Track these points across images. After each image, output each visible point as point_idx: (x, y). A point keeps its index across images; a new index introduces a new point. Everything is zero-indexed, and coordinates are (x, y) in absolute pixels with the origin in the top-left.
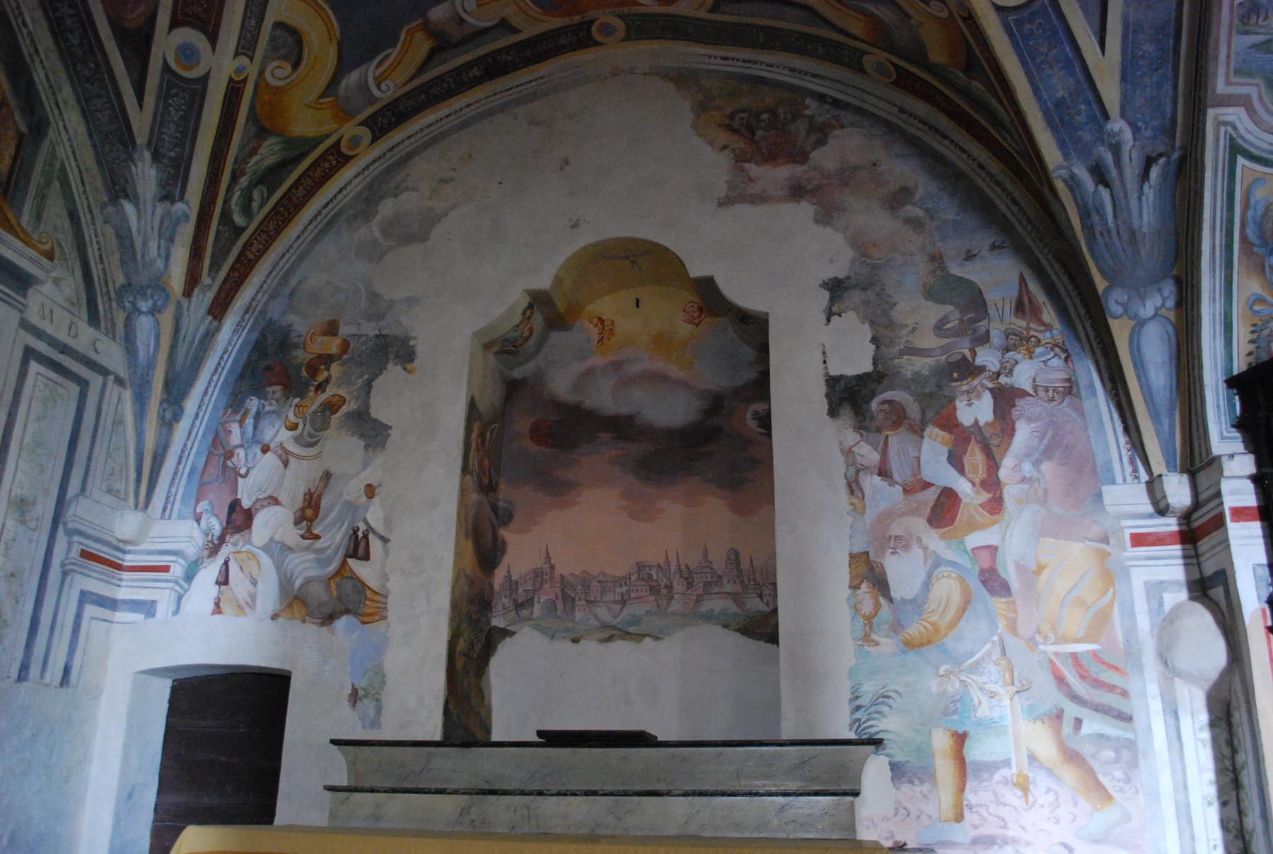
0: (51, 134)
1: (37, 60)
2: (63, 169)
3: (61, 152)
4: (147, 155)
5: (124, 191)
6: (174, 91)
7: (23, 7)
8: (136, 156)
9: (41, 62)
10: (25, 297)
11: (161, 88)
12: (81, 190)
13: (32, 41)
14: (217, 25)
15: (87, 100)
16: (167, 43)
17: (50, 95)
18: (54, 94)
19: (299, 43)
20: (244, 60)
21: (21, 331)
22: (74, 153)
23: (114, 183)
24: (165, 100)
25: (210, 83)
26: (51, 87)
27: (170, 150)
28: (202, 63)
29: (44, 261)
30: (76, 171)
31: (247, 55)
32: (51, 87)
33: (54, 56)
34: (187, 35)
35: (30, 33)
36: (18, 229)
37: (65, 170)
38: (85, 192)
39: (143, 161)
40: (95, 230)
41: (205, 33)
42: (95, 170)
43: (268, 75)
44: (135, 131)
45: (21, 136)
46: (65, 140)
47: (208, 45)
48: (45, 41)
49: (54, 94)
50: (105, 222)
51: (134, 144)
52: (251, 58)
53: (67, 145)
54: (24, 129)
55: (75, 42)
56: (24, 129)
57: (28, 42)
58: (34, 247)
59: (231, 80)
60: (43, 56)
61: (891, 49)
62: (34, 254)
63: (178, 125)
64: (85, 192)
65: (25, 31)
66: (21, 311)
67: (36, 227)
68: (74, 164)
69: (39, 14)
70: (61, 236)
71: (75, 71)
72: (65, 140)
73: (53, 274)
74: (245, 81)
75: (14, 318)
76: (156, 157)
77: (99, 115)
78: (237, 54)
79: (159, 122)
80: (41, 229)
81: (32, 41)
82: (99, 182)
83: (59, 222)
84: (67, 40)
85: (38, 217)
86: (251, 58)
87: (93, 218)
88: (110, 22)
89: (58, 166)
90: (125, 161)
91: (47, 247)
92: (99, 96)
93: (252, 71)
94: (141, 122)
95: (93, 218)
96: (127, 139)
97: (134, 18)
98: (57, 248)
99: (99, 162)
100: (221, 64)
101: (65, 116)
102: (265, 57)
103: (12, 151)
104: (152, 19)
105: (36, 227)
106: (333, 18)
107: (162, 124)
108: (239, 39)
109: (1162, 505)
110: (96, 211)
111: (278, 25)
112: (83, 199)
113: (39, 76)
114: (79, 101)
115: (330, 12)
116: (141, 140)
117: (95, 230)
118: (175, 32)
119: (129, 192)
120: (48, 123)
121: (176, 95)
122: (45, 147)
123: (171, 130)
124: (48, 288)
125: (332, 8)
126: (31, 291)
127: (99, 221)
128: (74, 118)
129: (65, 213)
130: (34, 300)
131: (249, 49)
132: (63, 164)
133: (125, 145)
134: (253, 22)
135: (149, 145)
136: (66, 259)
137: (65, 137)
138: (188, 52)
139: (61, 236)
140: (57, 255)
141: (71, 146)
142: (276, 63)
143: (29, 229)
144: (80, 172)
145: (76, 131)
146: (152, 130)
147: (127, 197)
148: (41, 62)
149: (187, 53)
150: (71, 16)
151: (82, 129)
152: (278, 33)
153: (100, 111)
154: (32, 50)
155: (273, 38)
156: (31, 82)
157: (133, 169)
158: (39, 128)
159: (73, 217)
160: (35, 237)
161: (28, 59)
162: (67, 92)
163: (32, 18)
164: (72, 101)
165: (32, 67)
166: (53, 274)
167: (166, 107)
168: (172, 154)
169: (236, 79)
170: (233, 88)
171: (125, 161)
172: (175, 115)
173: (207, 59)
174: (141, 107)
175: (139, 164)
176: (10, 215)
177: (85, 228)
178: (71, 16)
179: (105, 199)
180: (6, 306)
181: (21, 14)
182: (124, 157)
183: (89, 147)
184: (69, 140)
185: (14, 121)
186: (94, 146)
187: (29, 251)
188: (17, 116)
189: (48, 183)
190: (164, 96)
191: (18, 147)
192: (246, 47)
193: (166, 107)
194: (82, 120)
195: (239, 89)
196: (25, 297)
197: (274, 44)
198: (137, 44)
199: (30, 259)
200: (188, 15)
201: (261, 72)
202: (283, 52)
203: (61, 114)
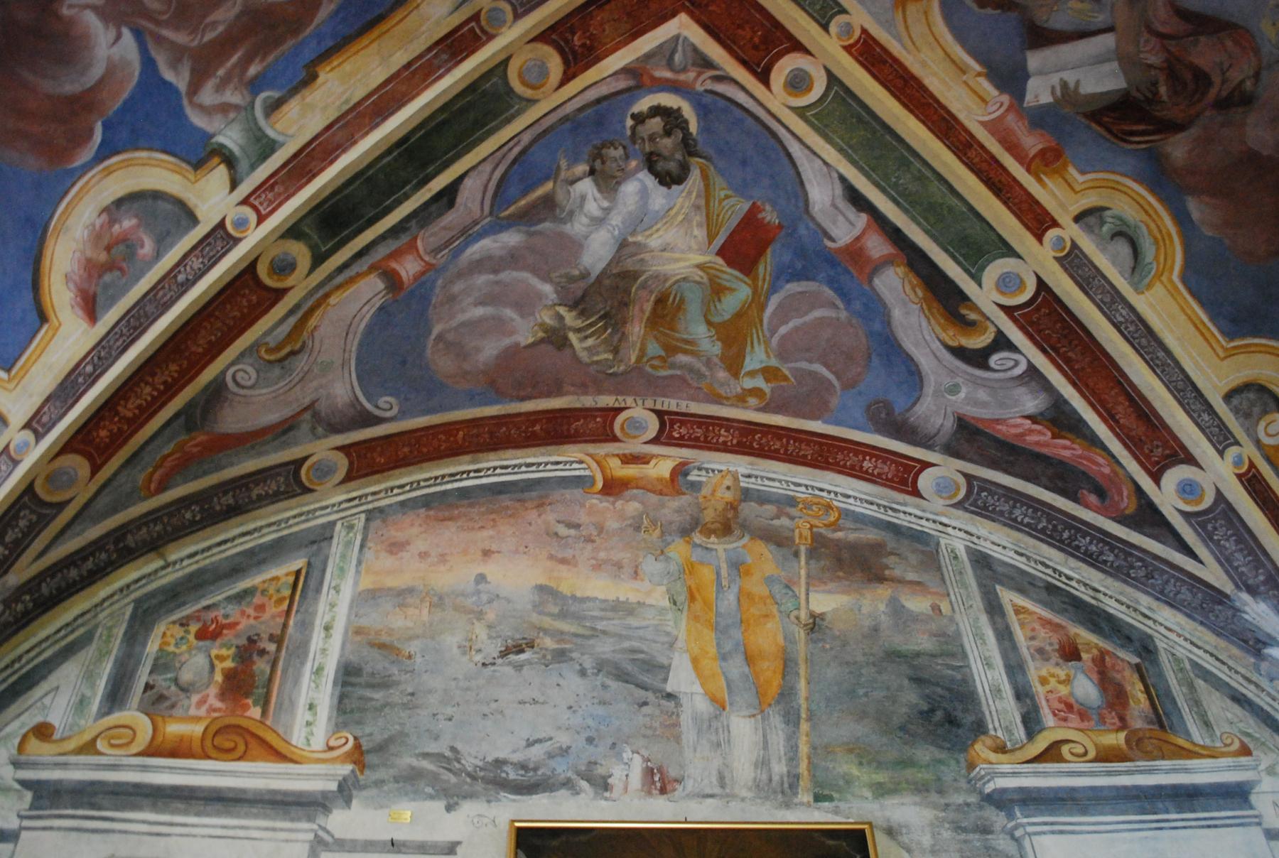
0: (1161, 645)
1: (1101, 596)
2: (1195, 665)
3: (1180, 652)
4: (1245, 596)
5: (1258, 641)
6: (1210, 527)
7: (1059, 568)
8: (1238, 604)
9: (1105, 594)
10: (1251, 808)
11: (1199, 534)
12: (1225, 668)
13: (1085, 585)
14: (1183, 447)
15: (1162, 592)
16: (1167, 495)
17: (1133, 614)
18: (1135, 610)
19: (1262, 389)
20: (1232, 452)
21: (1273, 843)
22: (1192, 643)
23: (1246, 642)
24: (1211, 539)
25: (1226, 494)
26: (1128, 607)
27: (1256, 576)
28: (1205, 486)
29: (1244, 760)
30: (1207, 657)
31: (1232, 445)
32: (1128, 607)
33: (1110, 581)
34: (1173, 477)
35: (1079, 582)
36: (1197, 749)
37: (1197, 664)
38: (1230, 668)
39: (1246, 604)
40: (1269, 694)
41: (1182, 462)
42: (1222, 643)
43: (1266, 441)
44: (1216, 585)
45: (1138, 668)
46: (1177, 639)
47: (1194, 469)
48: (1095, 577)
49: (1135, 610)
50: (1272, 680)
51: (1227, 596)
52: (1237, 443)
53: (1180, 641)
54: (1135, 660)
55: (1111, 558)
56: (1135, 660)
57: (1083, 589)
58: (1224, 755)
59: (1239, 476)
60: (1102, 589)
61: (335, 429)
62: (1229, 761)
63: (1241, 550)
64: (1230, 668)
65: (1074, 583)
66: (1259, 824)
67: (1212, 735)
68: (1200, 652)
69: (1073, 562)
70: (1241, 725)
71: (1133, 579)
72: (1177, 639)
73: (1262, 767)
74: (1252, 465)
75: (1256, 834)
76: (1252, 591)
77: (1179, 596)
78: (1221, 453)
79: (1225, 561)
80: (1218, 734)
81: (1085, 585)
82: (1235, 651)
83: (1229, 716)
84: (1105, 562)
85: (1207, 724)
86: (1237, 443)
87: (1257, 686)
88: (1119, 522)
89: (1188, 666)
90: (1234, 616)
91: (1236, 745)
92: (1167, 582)
93: (1249, 450)
94: (1212, 573)
95: (1257, 686)
96: (1219, 597)
97: (1128, 504)
98: (1246, 740)
99: (1218, 635)
100: (1218, 472)
101: (1161, 620)
102: (1247, 431)
103: (1140, 686)
104: (1139, 490)
105: (1212, 735)
106: (1263, 341)
107: (1228, 560)
108: (1210, 441)
109: (371, 759)
110: (1255, 677)
111: (1228, 397)
112: (1234, 676)
113: (1112, 607)
114: (1158, 599)
115: (1256, 341)
116: (1228, 588)
117: (1269, 694)
118: (1164, 481)
119: (1263, 639)
120: (1150, 637)
121: (1215, 529)
122: (1164, 658)
123: (1239, 559)
124: (1267, 784)
125: (1255, 336)
126: (1253, 798)
127: (1265, 683)
128: (1166, 615)
129: (1228, 701)
130: (1262, 802)
131: (1226, 439)
132: (1190, 660)
133: (1221, 603)
134: (1206, 417)
135: (1237, 586)
136: (1263, 744)
137: (1172, 636)
138: (1188, 488)
139: (1241, 725)
140: (1251, 746)
141: (1186, 639)
142: (1262, 424)
143: (1208, 742)
144: (1212, 655)
145: (1178, 624)
146: (1227, 572)
147: (1265, 644)
148: (1105, 594)
149: (1187, 489)
150: (1091, 543)
151: (1181, 618)
152: (1235, 401)
153: (1178, 592)
154: (1091, 593)
155: (1236, 411)
156: (1110, 618)
157: (1246, 617)
158: (1146, 648)
159: (1239, 699)
160: (1218, 744)
161: (1093, 602)
162: (1145, 601)
163: (1072, 569)
164: (1155, 604)
165: (1100, 605)
166: (1262, 767)
167: (1217, 543)
168: (1261, 578)
169: (1243, 470)
170: (1249, 481)
171: (1234, 616)
172: (1230, 545)
173: (1205, 481)
174: (1201, 562)
175: (1247, 609)
176: (1181, 742)
177: (1257, 700)
178: (1091, 543)
179: (1252, 660)
180: (1240, 829)
181: (1061, 574)
182: (1230, 613)
183: (1200, 628)
184: (1179, 635)
185: (1123, 660)
186: (1202, 623)
187: (1223, 762)
188: (1122, 654)
189: (1191, 686)
190: (1208, 537)
191: (1142, 679)
192: (1222, 439)
193: (1217, 543)
194: (1175, 612)
195: (1254, 476)
196: (1251, 808)
197: (1244, 415)
198: (1148, 517)
199: (1229, 769)
200: (1158, 463)
201: (1258, 443)
202: (1256, 410)
203: (1155, 621)
